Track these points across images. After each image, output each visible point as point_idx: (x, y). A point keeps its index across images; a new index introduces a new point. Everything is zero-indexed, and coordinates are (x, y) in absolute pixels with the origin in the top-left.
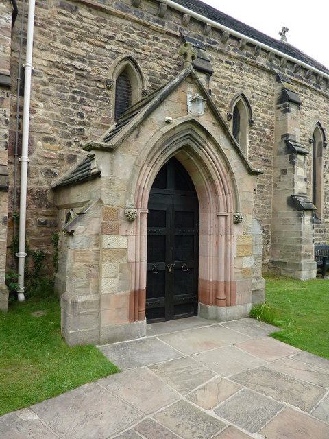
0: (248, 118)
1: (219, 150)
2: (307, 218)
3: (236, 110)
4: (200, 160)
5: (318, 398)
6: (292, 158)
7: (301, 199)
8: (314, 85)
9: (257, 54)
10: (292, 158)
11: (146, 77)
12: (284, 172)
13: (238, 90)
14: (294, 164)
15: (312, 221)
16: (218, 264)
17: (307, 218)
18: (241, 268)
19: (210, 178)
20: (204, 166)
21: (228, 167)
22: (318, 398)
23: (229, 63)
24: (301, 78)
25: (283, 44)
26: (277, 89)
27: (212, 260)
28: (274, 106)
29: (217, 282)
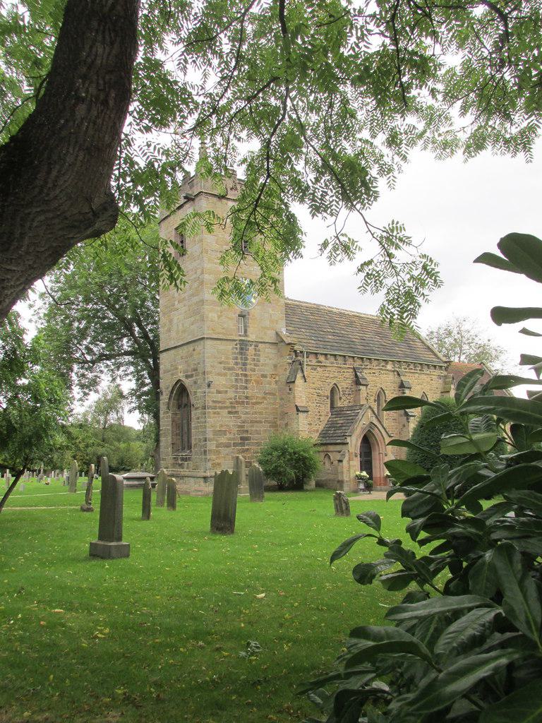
0: (384, 399)
1: (379, 430)
3: (378, 395)
4: (373, 434)
5: (260, 195)
6: (408, 419)
8: (420, 370)
9: (387, 364)
10: (408, 419)
11: (341, 390)
12: (404, 426)
13: (379, 386)
14: (409, 422)
16: (380, 471)
18: (45, 80)
19: (376, 439)
20: (375, 437)
21: (382, 436)
22: (260, 195)
23: (374, 373)
24: (411, 369)
25: (424, 690)
26: (397, 380)
27: (378, 470)
28: (397, 389)
29: (380, 477)
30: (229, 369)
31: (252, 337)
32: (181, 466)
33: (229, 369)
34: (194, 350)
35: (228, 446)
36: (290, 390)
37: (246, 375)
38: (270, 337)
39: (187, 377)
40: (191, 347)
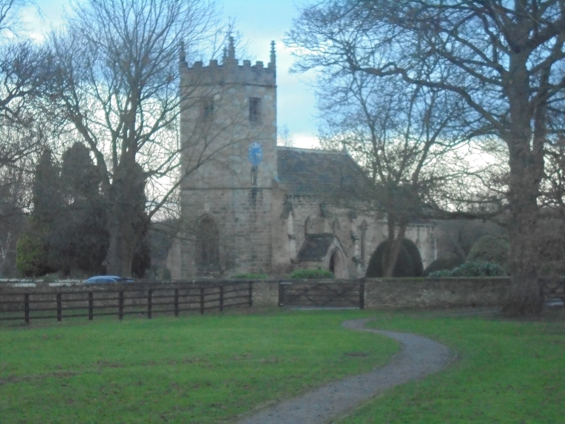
2: (359, 265)
7: (357, 258)
15: (361, 267)
17: (359, 265)
30: (247, 209)
31: (259, 185)
32: (207, 274)
33: (247, 209)
34: (222, 194)
35: (245, 261)
36: (283, 223)
37: (255, 213)
38: (268, 183)
39: (215, 212)
40: (219, 193)
